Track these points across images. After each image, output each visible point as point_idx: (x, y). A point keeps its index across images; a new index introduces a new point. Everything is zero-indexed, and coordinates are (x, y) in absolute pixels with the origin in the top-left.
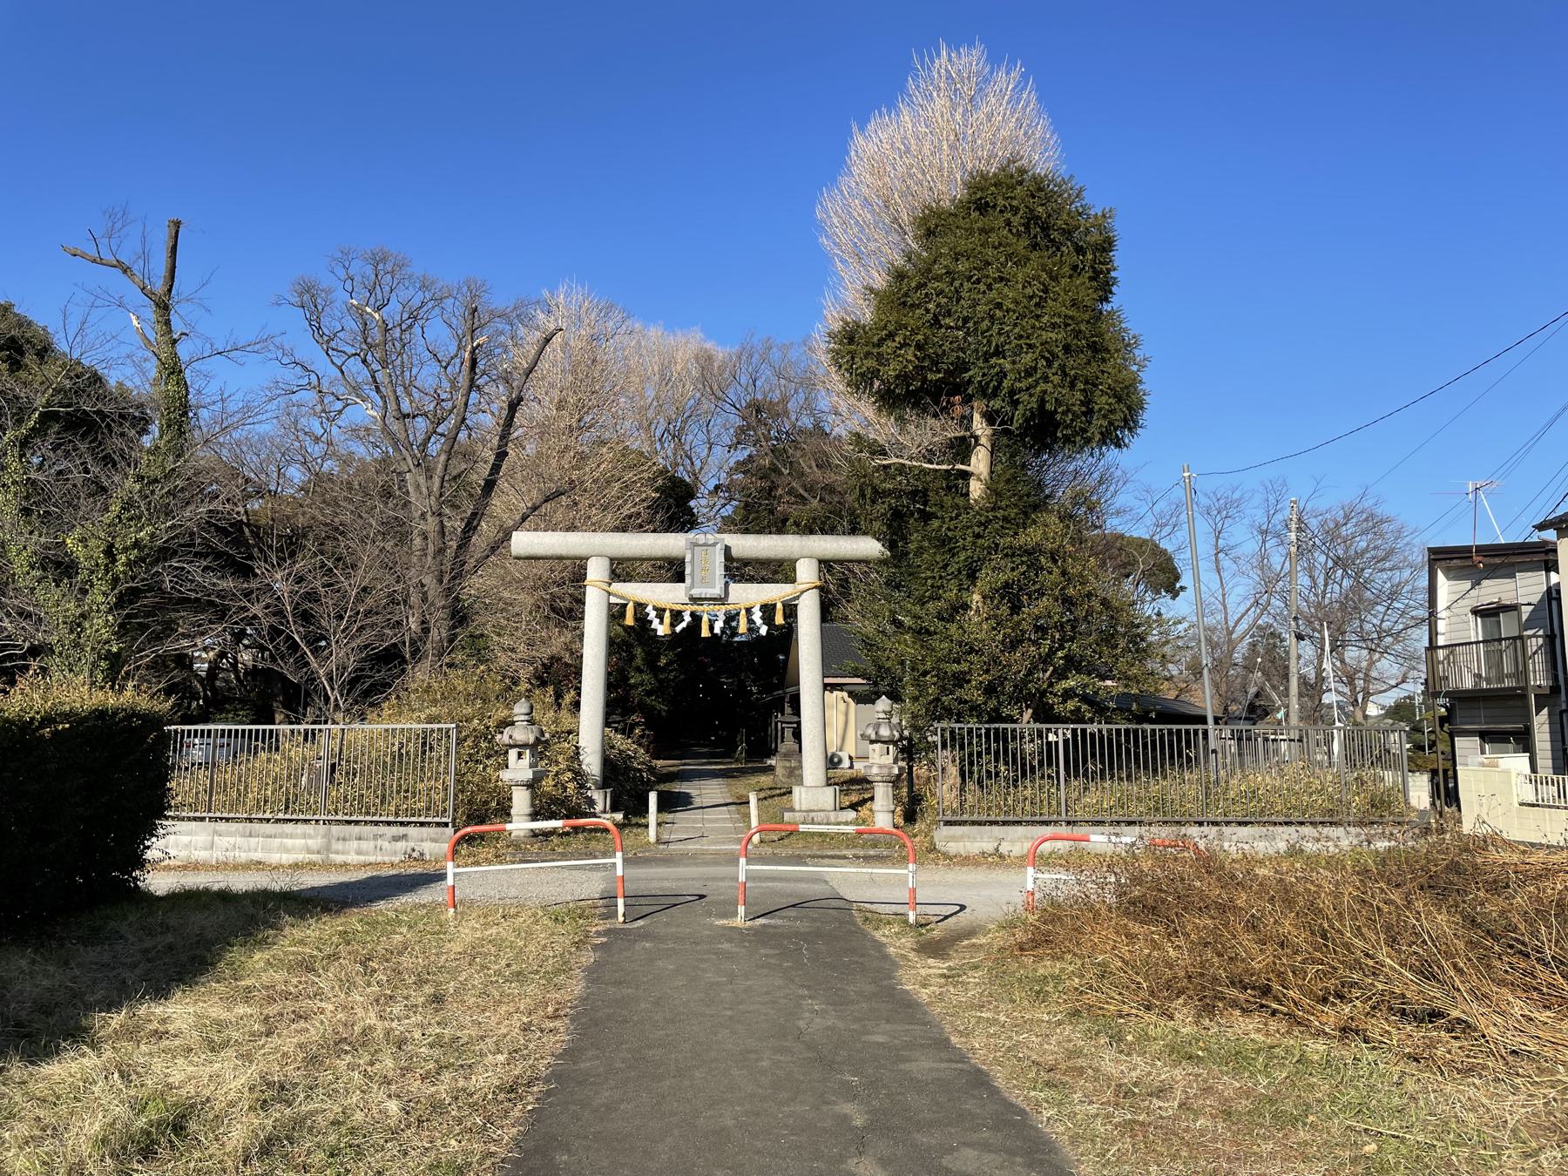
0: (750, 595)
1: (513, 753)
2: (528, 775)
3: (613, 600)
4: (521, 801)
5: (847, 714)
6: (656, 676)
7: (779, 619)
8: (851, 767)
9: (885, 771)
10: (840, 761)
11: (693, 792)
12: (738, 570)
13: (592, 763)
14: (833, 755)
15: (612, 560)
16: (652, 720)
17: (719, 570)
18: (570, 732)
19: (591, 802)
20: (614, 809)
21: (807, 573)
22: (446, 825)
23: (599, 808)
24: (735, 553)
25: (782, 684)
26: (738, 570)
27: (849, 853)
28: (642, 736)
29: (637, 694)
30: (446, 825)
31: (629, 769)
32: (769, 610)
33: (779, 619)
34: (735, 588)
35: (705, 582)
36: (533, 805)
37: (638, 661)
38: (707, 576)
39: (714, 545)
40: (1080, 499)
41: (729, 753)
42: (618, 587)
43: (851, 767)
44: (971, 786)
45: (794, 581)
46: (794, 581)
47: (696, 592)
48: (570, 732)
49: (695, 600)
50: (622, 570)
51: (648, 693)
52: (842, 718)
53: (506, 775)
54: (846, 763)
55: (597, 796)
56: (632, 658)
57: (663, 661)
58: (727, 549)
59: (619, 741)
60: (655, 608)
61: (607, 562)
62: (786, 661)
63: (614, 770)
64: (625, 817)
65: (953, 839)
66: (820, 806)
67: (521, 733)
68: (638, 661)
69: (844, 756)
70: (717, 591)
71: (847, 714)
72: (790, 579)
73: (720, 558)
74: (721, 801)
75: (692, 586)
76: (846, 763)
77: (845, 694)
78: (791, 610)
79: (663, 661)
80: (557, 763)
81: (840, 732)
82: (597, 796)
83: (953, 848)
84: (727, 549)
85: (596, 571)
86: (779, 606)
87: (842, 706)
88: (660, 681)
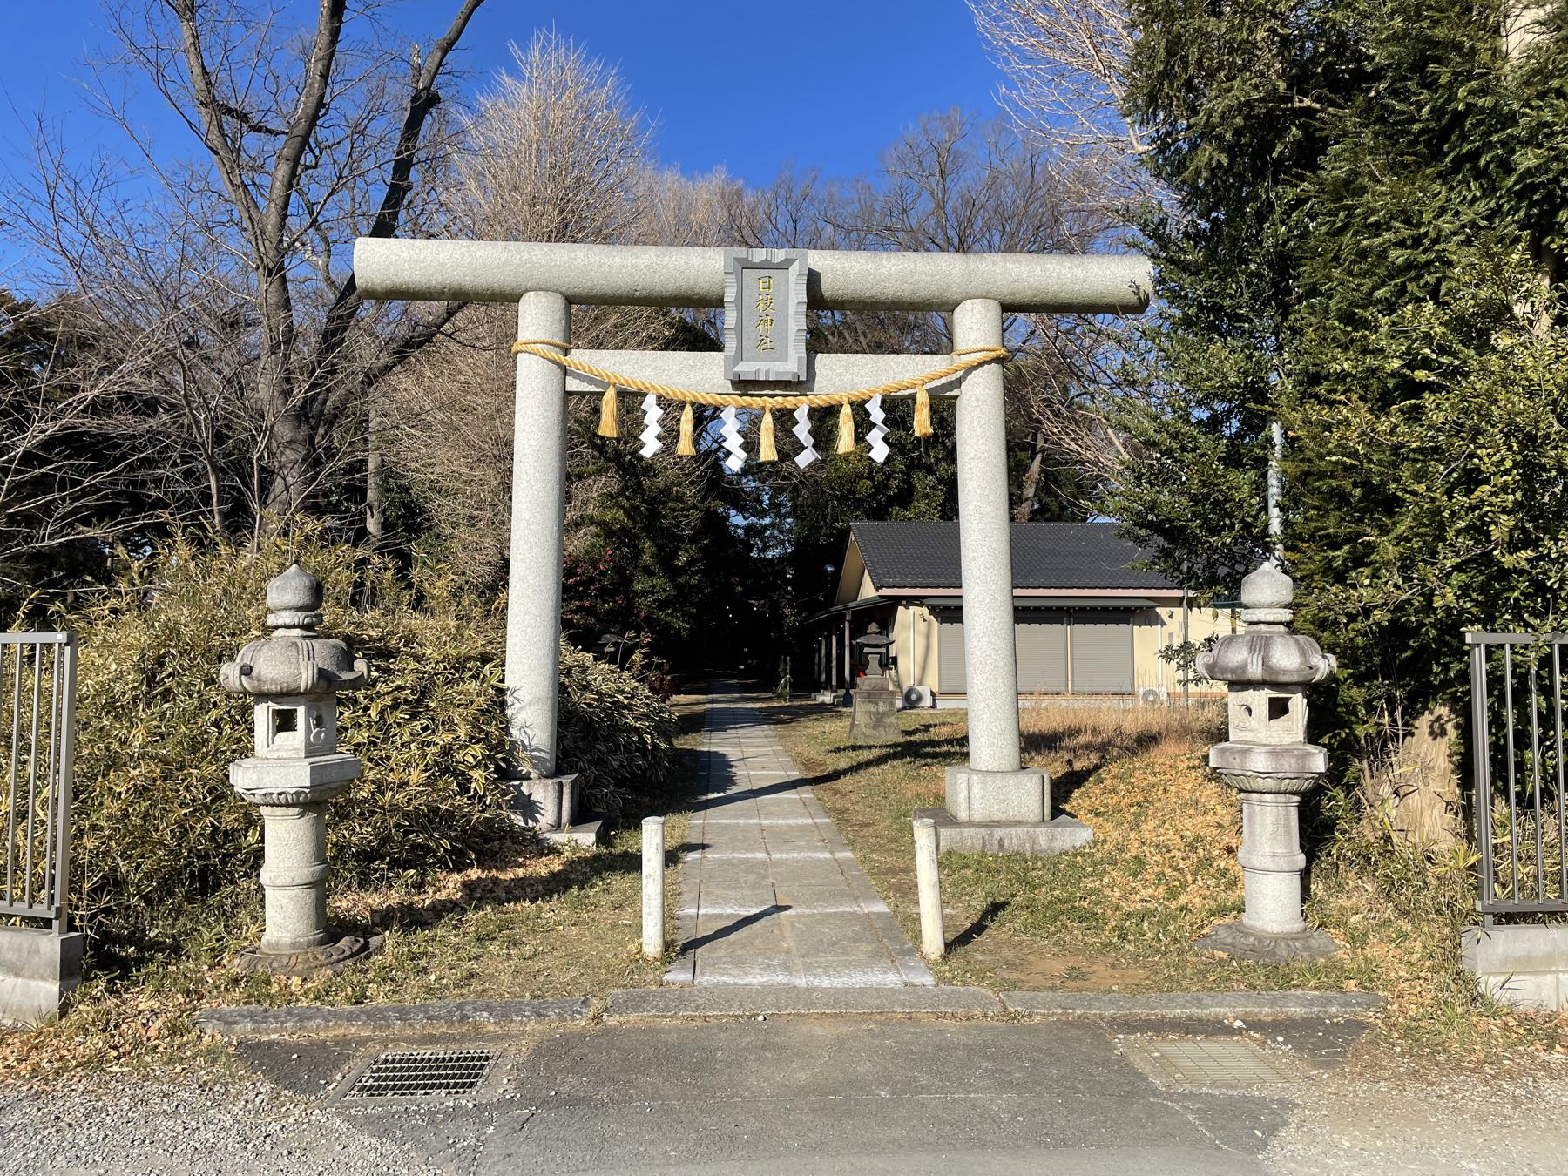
0: (851, 376)
1: (262, 715)
2: (299, 776)
3: (573, 385)
4: (287, 848)
5: (928, 636)
6: (672, 580)
7: (922, 424)
8: (934, 706)
9: (1289, 765)
10: (920, 699)
11: (732, 753)
12: (837, 322)
13: (531, 723)
14: (910, 691)
15: (570, 300)
16: (665, 643)
17: (796, 322)
18: (485, 659)
19: (527, 807)
20: (579, 818)
21: (975, 328)
22: (47, 924)
23: (546, 818)
24: (828, 286)
25: (831, 599)
26: (837, 322)
27: (1230, 1011)
28: (647, 667)
29: (644, 605)
30: (47, 924)
31: (616, 728)
32: (898, 409)
33: (922, 424)
34: (827, 363)
35: (765, 347)
36: (319, 856)
37: (647, 559)
38: (769, 330)
39: (785, 265)
40: (41, 1018)
41: (766, 683)
42: (581, 358)
43: (934, 706)
44: (1495, 810)
45: (950, 350)
46: (950, 350)
47: (747, 369)
48: (485, 659)
49: (743, 385)
50: (592, 315)
51: (662, 605)
52: (921, 642)
53: (242, 777)
54: (927, 702)
55: (542, 792)
56: (638, 553)
57: (683, 559)
58: (813, 279)
59: (601, 674)
60: (663, 402)
61: (559, 303)
62: (837, 574)
63: (581, 733)
64: (603, 838)
65: (1529, 965)
66: (1012, 814)
67: (282, 660)
68: (647, 559)
69: (925, 691)
70: (790, 365)
71: (928, 636)
72: (943, 343)
73: (798, 295)
74: (780, 776)
75: (739, 356)
76: (927, 702)
77: (925, 610)
78: (944, 409)
79: (683, 559)
80: (450, 725)
81: (919, 659)
82: (542, 792)
83: (1530, 992)
84: (813, 279)
85: (537, 320)
86: (923, 398)
87: (922, 626)
88: (679, 588)
